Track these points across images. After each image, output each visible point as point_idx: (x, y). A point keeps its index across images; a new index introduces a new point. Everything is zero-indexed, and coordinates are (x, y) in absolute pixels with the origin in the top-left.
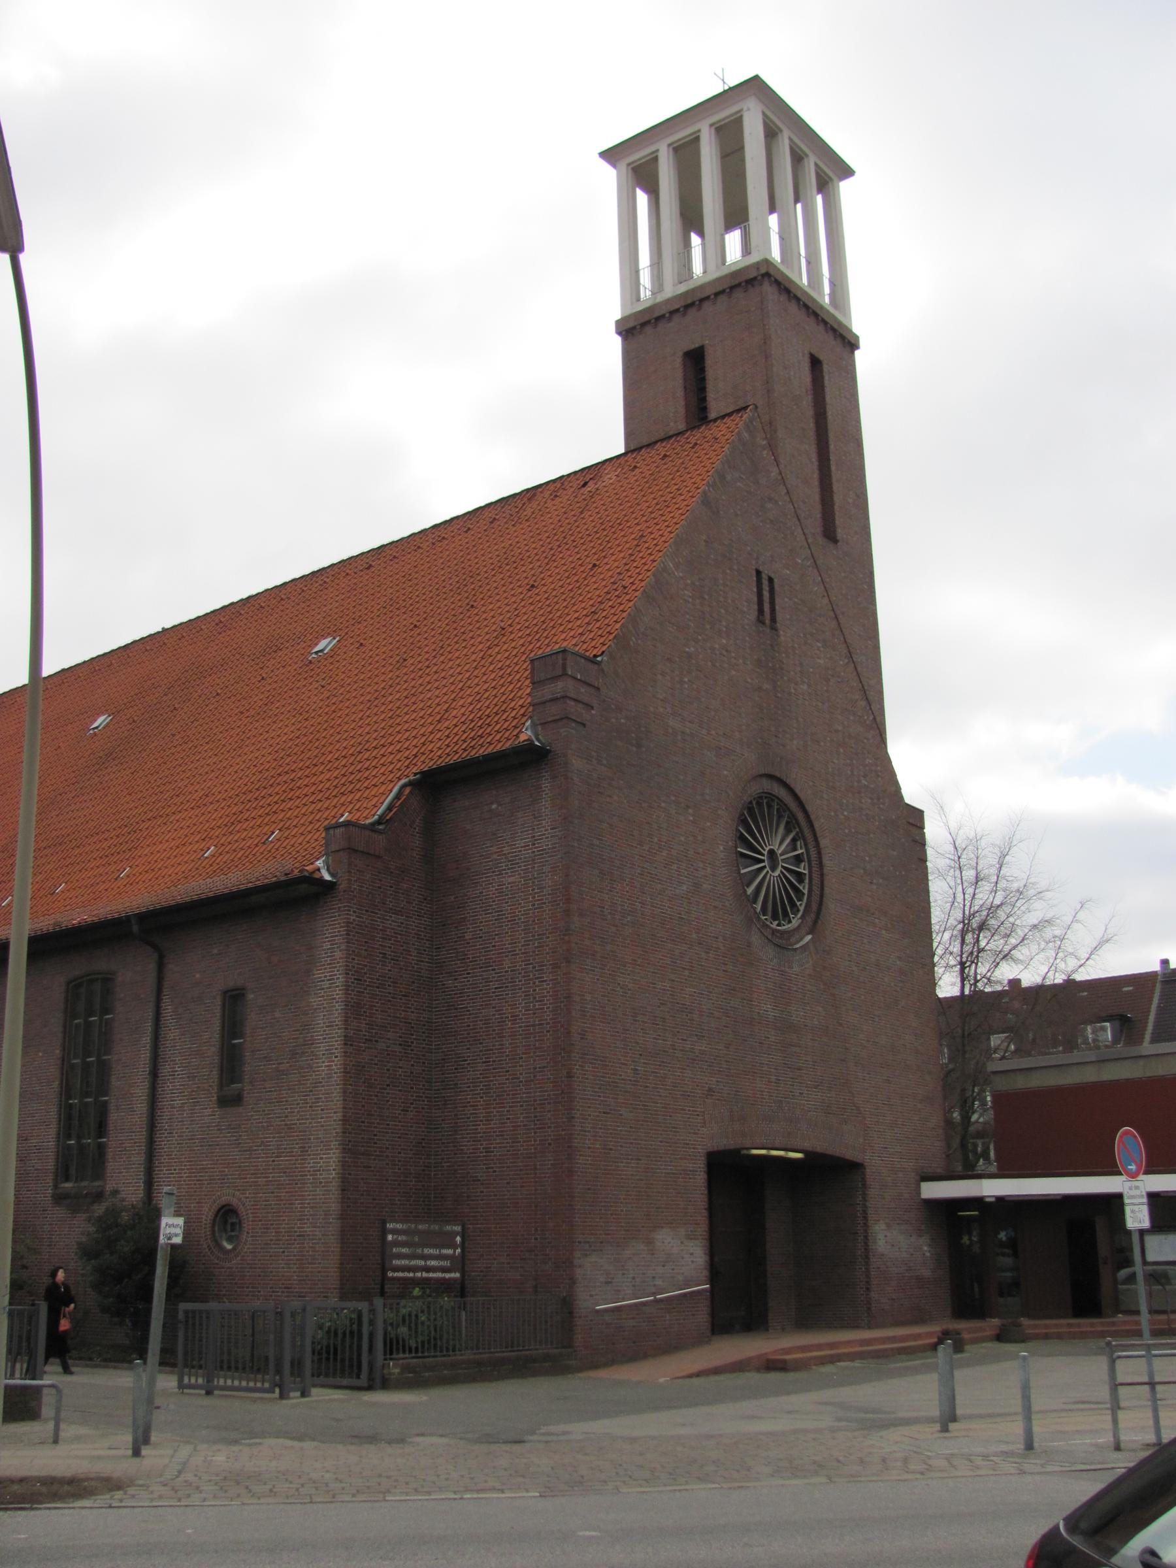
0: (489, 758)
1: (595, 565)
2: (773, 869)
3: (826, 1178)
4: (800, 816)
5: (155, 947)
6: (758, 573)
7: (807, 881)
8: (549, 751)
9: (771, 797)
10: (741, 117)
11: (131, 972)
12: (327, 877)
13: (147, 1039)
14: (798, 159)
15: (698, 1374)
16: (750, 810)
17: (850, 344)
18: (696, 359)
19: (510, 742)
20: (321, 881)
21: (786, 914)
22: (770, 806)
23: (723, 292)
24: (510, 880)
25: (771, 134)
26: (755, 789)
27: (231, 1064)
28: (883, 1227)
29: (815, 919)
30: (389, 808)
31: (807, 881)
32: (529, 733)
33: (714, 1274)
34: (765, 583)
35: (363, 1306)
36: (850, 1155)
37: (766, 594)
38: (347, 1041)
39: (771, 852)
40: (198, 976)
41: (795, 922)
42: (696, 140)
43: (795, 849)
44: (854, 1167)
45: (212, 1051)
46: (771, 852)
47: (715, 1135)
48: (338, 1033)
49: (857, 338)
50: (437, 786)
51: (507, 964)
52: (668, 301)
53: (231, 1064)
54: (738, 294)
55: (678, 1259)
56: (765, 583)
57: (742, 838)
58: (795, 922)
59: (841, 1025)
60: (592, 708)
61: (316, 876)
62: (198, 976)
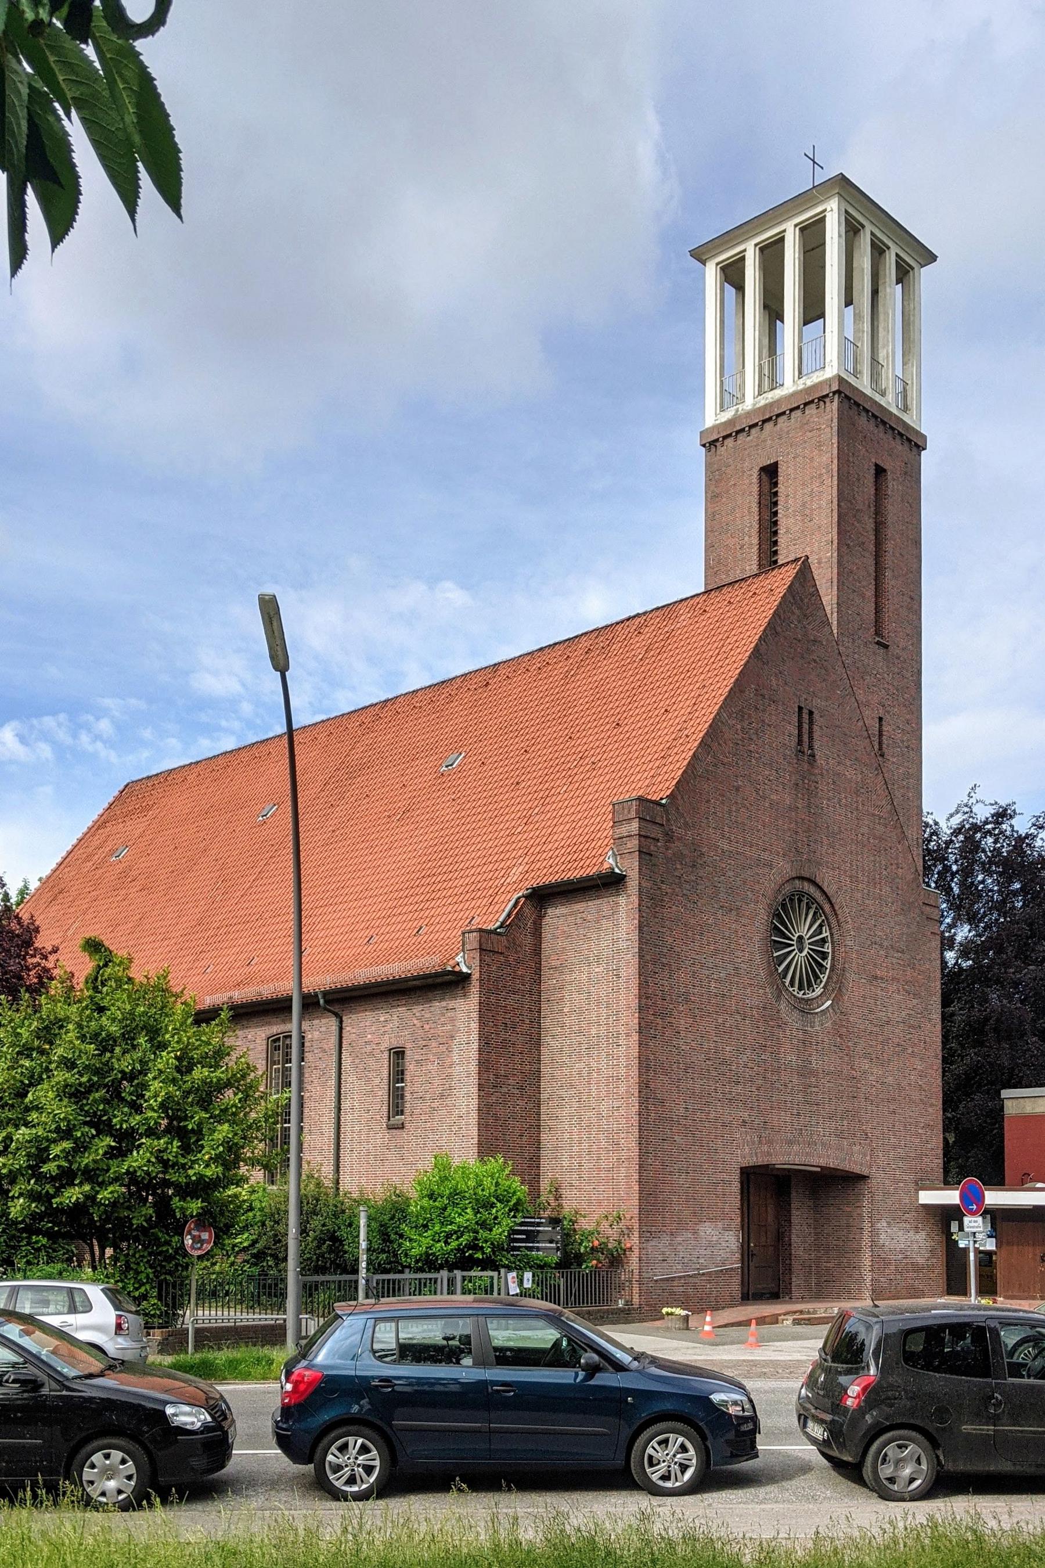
0: (581, 880)
1: (666, 711)
2: (801, 951)
3: (833, 1185)
4: (827, 907)
5: (336, 1015)
6: (800, 708)
7: (830, 958)
8: (625, 876)
9: (801, 894)
10: (825, 216)
11: (320, 1031)
12: (465, 970)
13: (333, 1082)
14: (878, 250)
15: (732, 1325)
16: (784, 906)
17: (915, 443)
18: (770, 472)
19: (596, 868)
20: (461, 972)
21: (810, 985)
22: (800, 901)
23: (798, 408)
24: (597, 970)
25: (852, 229)
26: (788, 888)
27: (397, 1103)
28: (885, 1224)
29: (836, 989)
30: (509, 915)
31: (830, 958)
32: (611, 861)
33: (747, 1253)
34: (805, 716)
35: (495, 1274)
36: (857, 1169)
37: (806, 726)
38: (481, 1087)
39: (800, 938)
40: (369, 1036)
41: (819, 991)
42: (780, 240)
43: (821, 933)
44: (862, 1178)
45: (382, 1093)
46: (800, 938)
47: (747, 1152)
48: (474, 1080)
49: (924, 437)
50: (543, 897)
51: (594, 1031)
52: (748, 414)
53: (397, 1103)
54: (811, 410)
55: (717, 1242)
56: (805, 716)
57: (776, 928)
58: (819, 991)
59: (854, 1070)
60: (658, 840)
61: (457, 969)
62: (369, 1036)
